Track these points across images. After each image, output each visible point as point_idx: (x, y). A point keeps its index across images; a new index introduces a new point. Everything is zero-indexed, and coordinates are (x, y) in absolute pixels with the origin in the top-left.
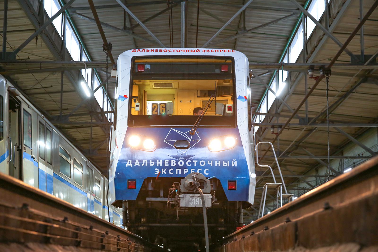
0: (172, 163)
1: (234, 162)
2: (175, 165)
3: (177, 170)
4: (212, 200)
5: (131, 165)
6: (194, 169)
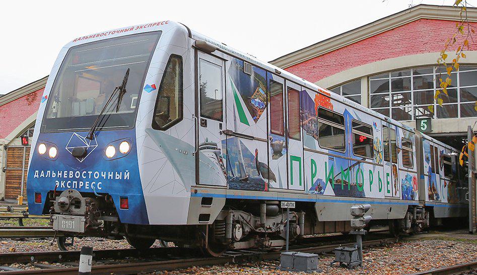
0: (70, 174)
1: (127, 173)
2: (72, 177)
3: (74, 182)
4: (86, 223)
5: (38, 176)
6: (88, 183)
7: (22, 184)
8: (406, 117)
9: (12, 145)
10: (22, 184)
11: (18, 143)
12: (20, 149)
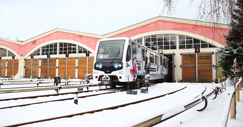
4: (110, 82)
7: (32, 72)
8: (156, 49)
9: (27, 58)
10: (32, 72)
11: (30, 58)
12: (30, 60)
